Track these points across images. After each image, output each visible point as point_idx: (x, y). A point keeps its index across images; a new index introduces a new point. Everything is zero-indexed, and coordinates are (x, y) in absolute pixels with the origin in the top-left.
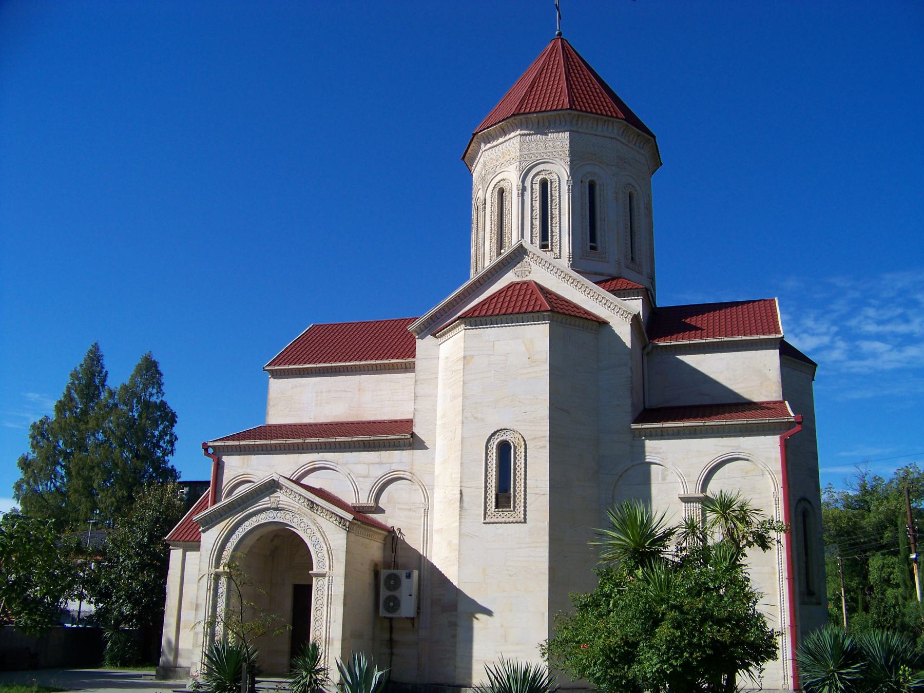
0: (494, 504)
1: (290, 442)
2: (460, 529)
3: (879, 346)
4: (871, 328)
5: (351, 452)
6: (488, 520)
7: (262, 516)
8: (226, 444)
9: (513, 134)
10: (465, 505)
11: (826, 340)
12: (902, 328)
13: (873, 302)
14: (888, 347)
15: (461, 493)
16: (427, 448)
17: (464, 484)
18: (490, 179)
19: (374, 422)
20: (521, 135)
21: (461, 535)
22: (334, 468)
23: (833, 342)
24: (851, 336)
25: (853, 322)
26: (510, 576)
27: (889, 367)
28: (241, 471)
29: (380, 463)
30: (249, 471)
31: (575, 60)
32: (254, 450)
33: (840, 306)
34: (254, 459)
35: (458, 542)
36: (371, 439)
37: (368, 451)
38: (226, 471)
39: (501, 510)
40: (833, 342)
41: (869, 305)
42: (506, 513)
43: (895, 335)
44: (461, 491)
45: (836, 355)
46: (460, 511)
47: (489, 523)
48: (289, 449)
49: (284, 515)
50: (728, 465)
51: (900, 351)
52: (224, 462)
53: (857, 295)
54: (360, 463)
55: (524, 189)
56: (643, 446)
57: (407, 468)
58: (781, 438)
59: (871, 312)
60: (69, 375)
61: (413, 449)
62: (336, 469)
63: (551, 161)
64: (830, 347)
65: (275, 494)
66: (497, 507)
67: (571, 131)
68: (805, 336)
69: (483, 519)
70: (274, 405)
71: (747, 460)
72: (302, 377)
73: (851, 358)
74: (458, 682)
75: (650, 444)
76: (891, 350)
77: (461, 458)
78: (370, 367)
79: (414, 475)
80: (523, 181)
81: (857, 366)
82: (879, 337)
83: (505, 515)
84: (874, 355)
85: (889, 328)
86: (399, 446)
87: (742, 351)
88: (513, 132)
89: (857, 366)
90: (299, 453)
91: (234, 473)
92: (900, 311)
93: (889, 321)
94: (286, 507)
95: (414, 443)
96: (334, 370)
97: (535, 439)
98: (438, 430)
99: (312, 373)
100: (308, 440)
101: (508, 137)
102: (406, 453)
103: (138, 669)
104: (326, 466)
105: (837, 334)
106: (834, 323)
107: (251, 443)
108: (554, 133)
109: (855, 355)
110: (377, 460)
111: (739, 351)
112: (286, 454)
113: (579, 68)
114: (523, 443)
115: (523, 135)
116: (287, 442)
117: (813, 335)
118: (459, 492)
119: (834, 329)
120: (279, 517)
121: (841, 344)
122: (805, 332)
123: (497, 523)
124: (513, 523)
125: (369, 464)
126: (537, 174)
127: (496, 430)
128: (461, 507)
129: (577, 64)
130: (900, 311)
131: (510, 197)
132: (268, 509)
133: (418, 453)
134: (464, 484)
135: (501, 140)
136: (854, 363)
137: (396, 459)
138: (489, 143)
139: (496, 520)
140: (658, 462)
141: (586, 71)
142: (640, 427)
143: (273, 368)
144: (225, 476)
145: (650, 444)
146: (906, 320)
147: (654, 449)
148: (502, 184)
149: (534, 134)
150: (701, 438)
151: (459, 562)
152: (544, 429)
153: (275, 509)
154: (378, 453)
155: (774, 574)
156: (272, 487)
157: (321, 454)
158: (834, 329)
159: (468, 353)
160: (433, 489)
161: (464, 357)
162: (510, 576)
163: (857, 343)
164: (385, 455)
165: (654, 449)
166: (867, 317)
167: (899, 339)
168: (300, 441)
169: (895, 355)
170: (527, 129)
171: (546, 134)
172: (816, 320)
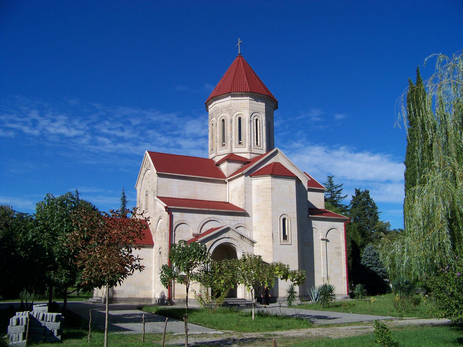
2: (273, 246)
3: (106, 140)
4: (105, 131)
5: (224, 215)
6: (281, 244)
7: (224, 239)
8: (176, 208)
9: (245, 98)
10: (274, 238)
11: (82, 133)
12: (120, 134)
13: (111, 119)
19: (209, 201)
20: (250, 99)
21: (273, 248)
24: (94, 133)
25: (97, 127)
28: (181, 219)
30: (184, 219)
31: (241, 66)
33: (94, 118)
34: (186, 215)
37: (230, 216)
43: (115, 136)
45: (84, 141)
48: (187, 211)
51: (115, 145)
54: (227, 220)
56: (311, 222)
57: (243, 223)
58: (344, 223)
59: (107, 123)
61: (245, 216)
64: (82, 137)
65: (228, 232)
68: (73, 129)
72: (171, 178)
75: (313, 222)
76: (111, 144)
81: (93, 148)
82: (108, 136)
83: (285, 242)
84: (103, 144)
86: (241, 215)
89: (93, 148)
90: (204, 214)
92: (121, 125)
95: (244, 214)
96: (183, 177)
100: (210, 210)
101: (243, 98)
102: (243, 218)
104: (211, 219)
105: (88, 131)
106: (88, 125)
109: (94, 143)
110: (233, 219)
112: (199, 214)
113: (241, 70)
115: (251, 100)
118: (271, 234)
119: (88, 128)
121: (88, 136)
122: (73, 126)
125: (230, 220)
126: (255, 116)
128: (273, 239)
129: (241, 68)
130: (121, 125)
132: (225, 237)
133: (247, 218)
135: (239, 98)
137: (240, 219)
144: (174, 221)
145: (313, 222)
146: (122, 130)
147: (315, 223)
150: (326, 221)
152: (295, 215)
153: (227, 238)
154: (233, 217)
156: (227, 229)
157: (213, 215)
158: (88, 128)
164: (236, 218)
165: (315, 223)
166: (105, 125)
168: (207, 209)
169: (112, 146)
171: (258, 102)
172: (80, 122)
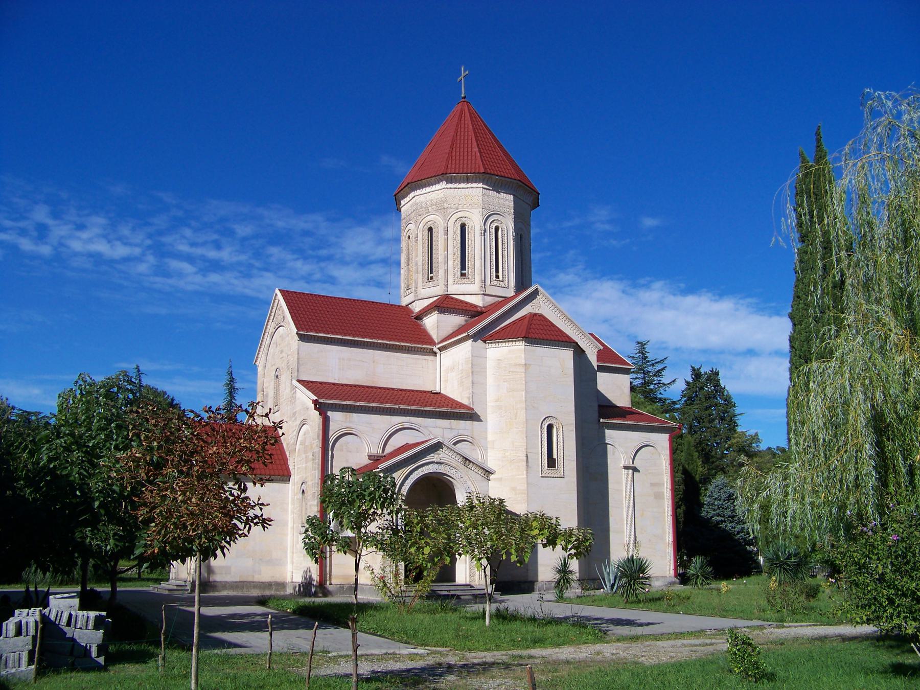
3: (186, 267)
4: (184, 248)
5: (431, 418)
6: (543, 475)
7: (425, 468)
9: (474, 185)
10: (530, 464)
11: (137, 251)
12: (212, 254)
13: (193, 223)
16: (482, 421)
20: (483, 188)
21: (528, 484)
23: (143, 254)
24: (162, 252)
25: (167, 239)
27: (190, 288)
28: (345, 425)
29: (451, 429)
30: (351, 425)
32: (383, 411)
33: (161, 221)
34: (355, 416)
38: (331, 423)
40: (143, 254)
41: (189, 226)
43: (203, 258)
45: (142, 268)
48: (376, 411)
53: (180, 214)
59: (188, 232)
61: (473, 420)
64: (139, 259)
68: (118, 243)
73: (156, 274)
74: (530, 579)
75: (608, 433)
76: (196, 273)
81: (160, 282)
82: (190, 259)
83: (552, 473)
84: (180, 275)
85: (199, 251)
89: (160, 282)
90: (391, 415)
91: (339, 426)
92: (215, 237)
93: (204, 244)
95: (470, 415)
96: (379, 345)
98: (489, 410)
99: (334, 342)
101: (469, 185)
103: (73, 586)
104: (405, 426)
105: (149, 247)
106: (150, 236)
108: (504, 193)
110: (449, 427)
117: (126, 244)
119: (149, 242)
120: (440, 469)
121: (151, 259)
122: (119, 239)
125: (443, 429)
126: (493, 221)
133: (476, 423)
134: (529, 451)
135: (462, 185)
136: (158, 279)
145: (608, 433)
146: (218, 246)
148: (464, 220)
149: (492, 190)
151: (527, 501)
153: (437, 463)
156: (437, 446)
158: (149, 242)
161: (525, 364)
163: (167, 260)
164: (454, 423)
166: (183, 237)
167: (207, 264)
169: (199, 279)
170: (486, 185)
171: (499, 192)
172: (134, 229)
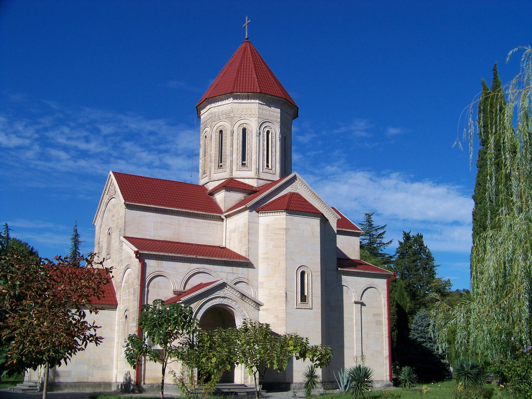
0: (300, 300)
1: (188, 257)
3: (63, 155)
4: (62, 141)
6: (297, 307)
7: (218, 300)
8: (151, 253)
10: (288, 299)
11: (27, 142)
12: (83, 146)
13: (71, 124)
14: (68, 157)
15: (286, 294)
16: (255, 268)
17: (287, 290)
18: (237, 120)
22: (209, 273)
25: (50, 134)
26: (307, 333)
28: (157, 269)
29: (233, 273)
30: (161, 269)
34: (165, 263)
35: (285, 316)
36: (231, 260)
37: (227, 266)
39: (303, 303)
42: (304, 304)
43: (76, 149)
44: (286, 292)
45: (30, 154)
46: (286, 302)
47: (298, 308)
48: (180, 260)
49: (227, 301)
50: (372, 288)
51: (75, 161)
52: (146, 263)
55: (260, 134)
57: (245, 277)
59: (66, 130)
60: (448, 278)
62: (211, 274)
63: (272, 122)
66: (301, 301)
67: (281, 109)
69: (296, 306)
70: (128, 225)
71: (375, 288)
72: (145, 211)
75: (344, 277)
76: (69, 160)
77: (286, 277)
78: (196, 214)
79: (249, 280)
80: (259, 129)
81: (42, 165)
82: (65, 149)
84: (58, 160)
85: (73, 143)
87: (347, 235)
88: (254, 99)
89: (42, 165)
90: (190, 263)
92: (86, 133)
94: (229, 296)
95: (247, 264)
97: (315, 271)
100: (198, 257)
101: (249, 101)
104: (205, 271)
105: (36, 140)
106: (38, 131)
107: (166, 255)
108: (273, 107)
109: (44, 157)
110: (231, 271)
111: (346, 235)
114: (311, 273)
115: (261, 104)
116: (187, 256)
119: (36, 136)
121: (37, 148)
122: (15, 133)
123: (301, 309)
124: (308, 309)
125: (227, 273)
127: (300, 265)
128: (286, 300)
130: (86, 133)
131: (250, 134)
133: (250, 270)
138: (237, 99)
139: (301, 307)
140: (346, 285)
141: (265, 69)
142: (342, 270)
143: (130, 203)
145: (344, 277)
146: (87, 140)
147: (346, 280)
148: (245, 126)
149: (265, 105)
153: (223, 297)
155: (383, 335)
156: (223, 285)
157: (202, 265)
158: (36, 136)
159: (287, 227)
160: (258, 288)
162: (307, 333)
165: (346, 280)
166: (63, 133)
169: (71, 163)
170: (261, 101)
171: (270, 107)
